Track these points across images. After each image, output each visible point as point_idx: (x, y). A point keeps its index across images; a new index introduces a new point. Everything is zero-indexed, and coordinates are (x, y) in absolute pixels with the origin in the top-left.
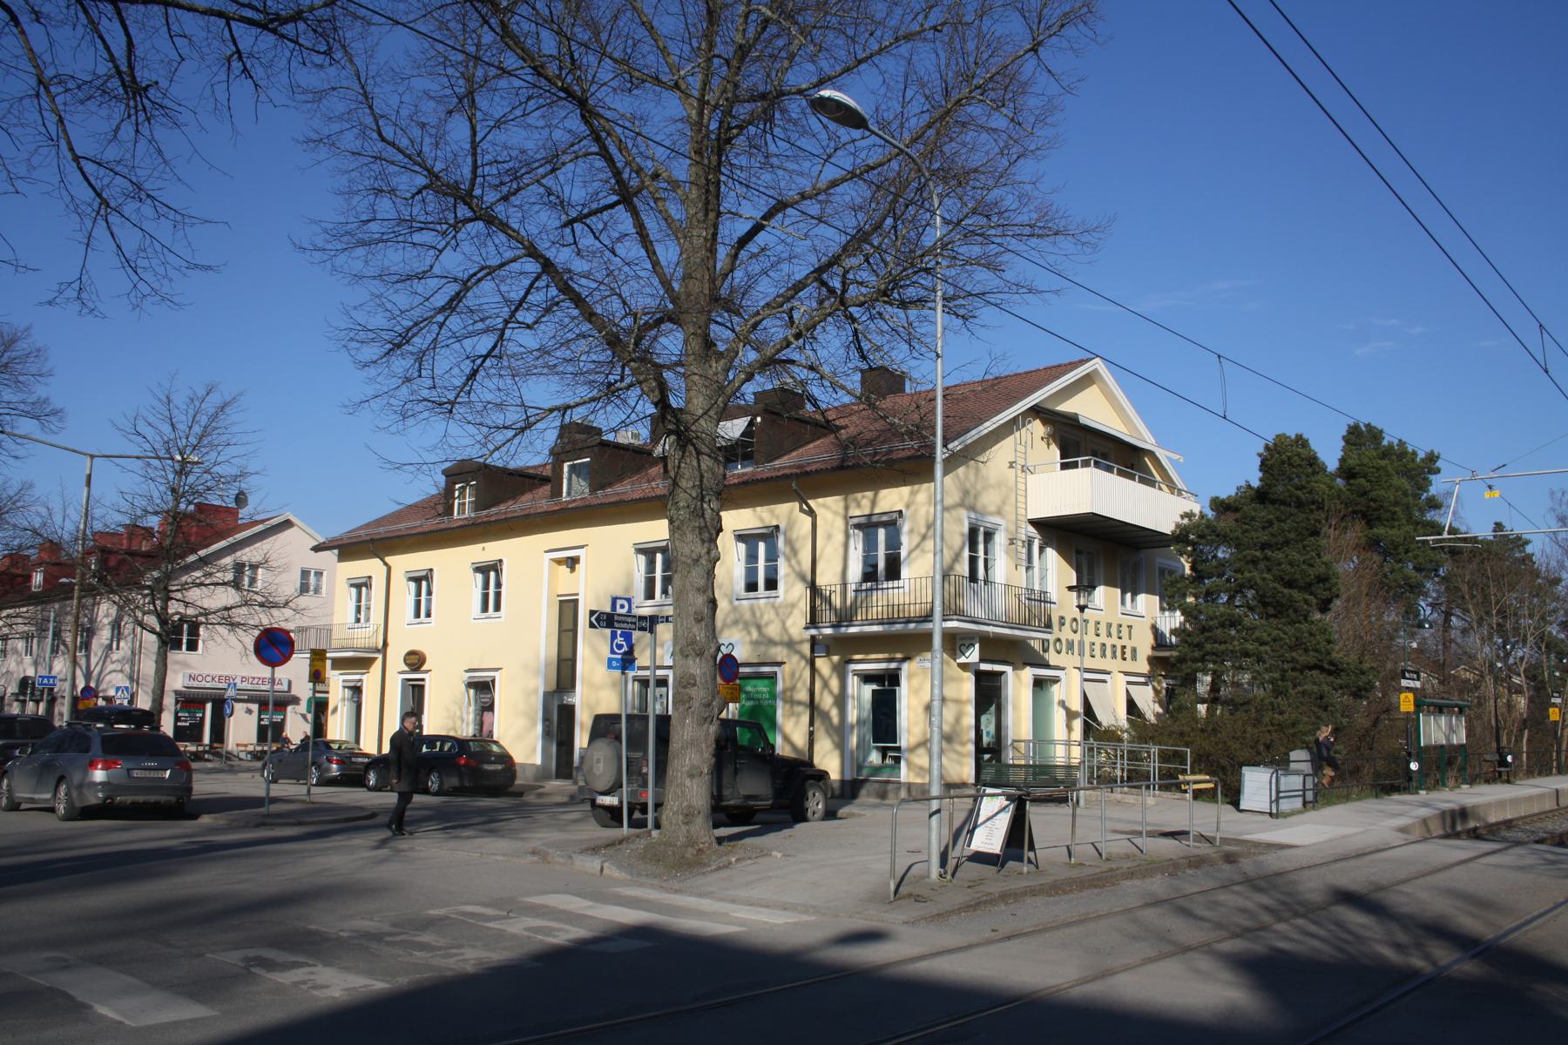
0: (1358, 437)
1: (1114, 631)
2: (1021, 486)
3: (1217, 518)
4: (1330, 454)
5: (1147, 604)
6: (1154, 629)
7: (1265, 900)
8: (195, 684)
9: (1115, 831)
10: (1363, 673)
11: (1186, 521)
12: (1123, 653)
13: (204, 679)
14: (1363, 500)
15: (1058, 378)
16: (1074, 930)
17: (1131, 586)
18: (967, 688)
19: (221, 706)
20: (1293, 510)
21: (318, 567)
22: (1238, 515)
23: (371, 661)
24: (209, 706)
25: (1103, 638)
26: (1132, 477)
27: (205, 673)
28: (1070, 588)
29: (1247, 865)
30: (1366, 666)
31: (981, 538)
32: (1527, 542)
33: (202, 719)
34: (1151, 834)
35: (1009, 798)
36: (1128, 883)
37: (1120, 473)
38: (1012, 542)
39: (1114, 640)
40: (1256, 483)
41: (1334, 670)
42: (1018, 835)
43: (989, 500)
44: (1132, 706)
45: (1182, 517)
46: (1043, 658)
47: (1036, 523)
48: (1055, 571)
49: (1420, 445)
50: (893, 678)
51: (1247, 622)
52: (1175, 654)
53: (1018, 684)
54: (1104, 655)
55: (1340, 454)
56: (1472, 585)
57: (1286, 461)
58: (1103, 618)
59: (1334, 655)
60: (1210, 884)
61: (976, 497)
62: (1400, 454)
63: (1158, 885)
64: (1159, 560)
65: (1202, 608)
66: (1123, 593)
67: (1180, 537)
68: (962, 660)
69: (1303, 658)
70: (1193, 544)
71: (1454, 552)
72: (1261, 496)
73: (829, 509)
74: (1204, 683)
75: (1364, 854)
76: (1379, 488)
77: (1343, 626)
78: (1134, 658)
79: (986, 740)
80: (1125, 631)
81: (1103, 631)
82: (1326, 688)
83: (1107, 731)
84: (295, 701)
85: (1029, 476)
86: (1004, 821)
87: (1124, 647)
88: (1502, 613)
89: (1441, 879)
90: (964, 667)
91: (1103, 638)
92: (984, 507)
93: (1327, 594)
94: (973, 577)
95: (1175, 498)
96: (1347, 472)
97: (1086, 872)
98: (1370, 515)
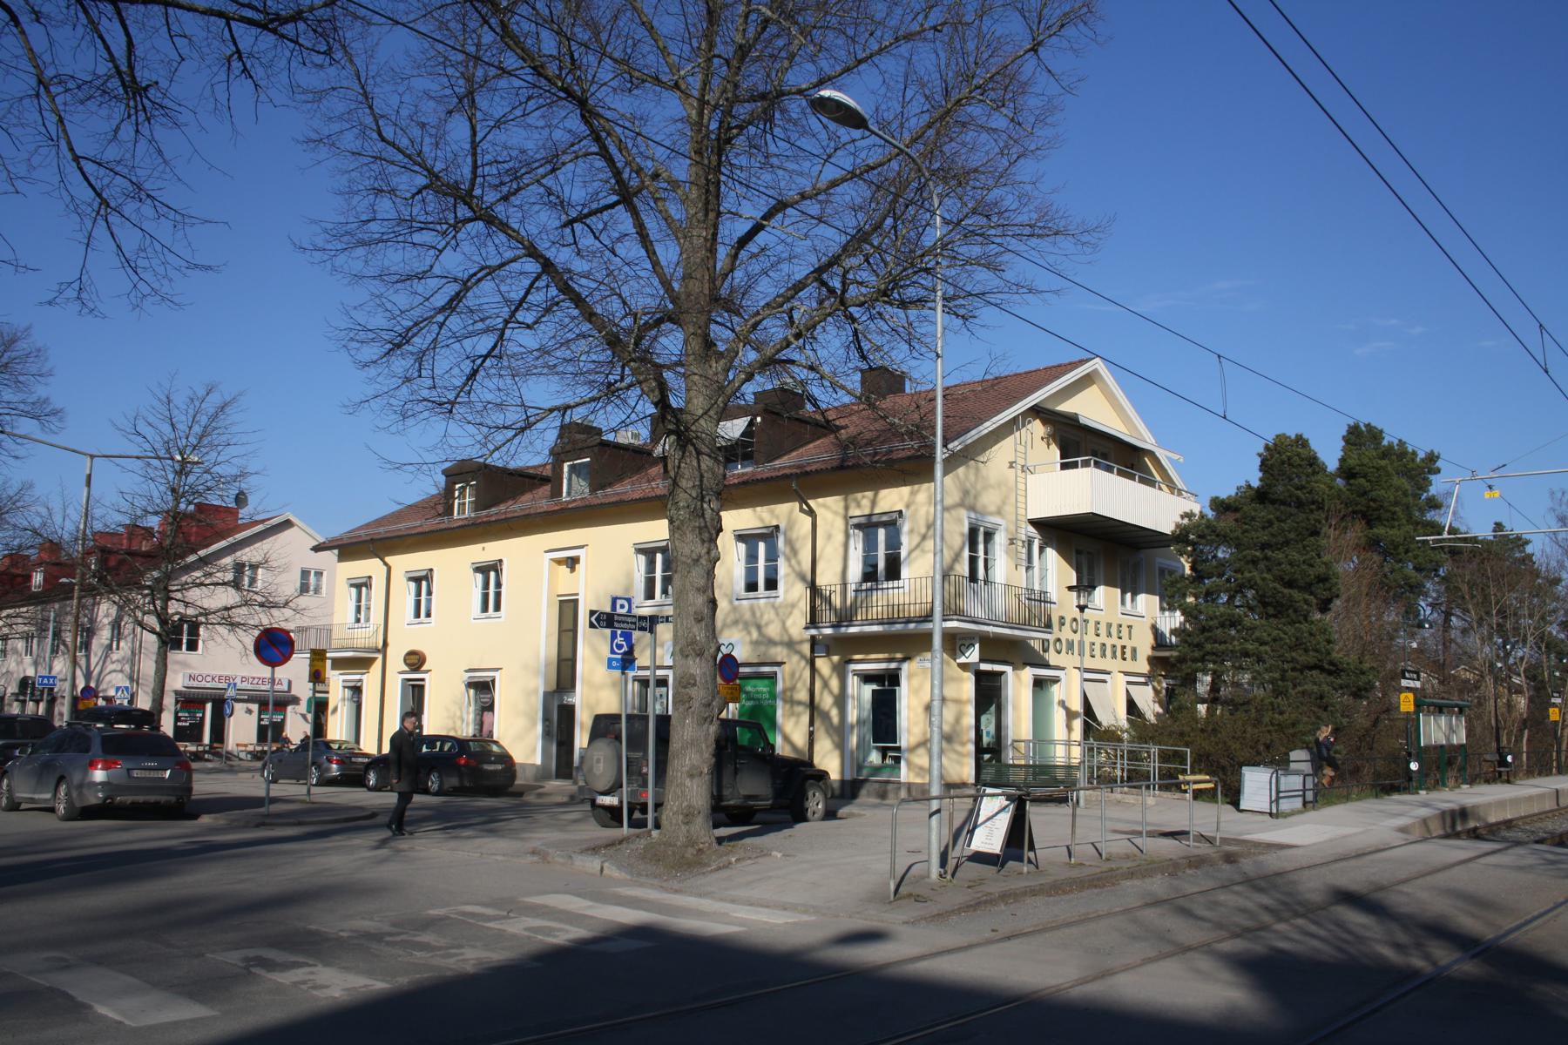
0: (1358, 437)
1: (1114, 631)
2: (1021, 486)
3: (1217, 518)
4: (1330, 454)
5: (1147, 604)
6: (1154, 629)
7: (1265, 900)
8: (195, 684)
9: (1115, 831)
10: (1363, 673)
11: (1186, 521)
12: (1123, 653)
13: (204, 679)
14: (1363, 500)
15: (1058, 378)
16: (1074, 930)
17: (1131, 586)
18: (967, 688)
19: (221, 706)
20: (1293, 510)
21: (318, 567)
22: (1238, 515)
23: (371, 661)
24: (209, 706)
25: (1103, 638)
26: (1132, 477)
27: (205, 673)
28: (1070, 588)
29: (1247, 865)
30: (1366, 666)
31: (981, 538)
32: (1527, 542)
33: (202, 719)
34: (1151, 834)
35: (1009, 798)
36: (1128, 883)
37: (1120, 473)
38: (1012, 542)
39: (1114, 640)
40: (1256, 483)
41: (1334, 670)
42: (1018, 835)
43: (989, 500)
44: (1132, 706)
45: (1182, 517)
46: (1043, 658)
47: (1036, 523)
48: (1055, 571)
49: (1420, 445)
50: (893, 678)
51: (1247, 622)
52: (1175, 654)
53: (1018, 684)
54: (1104, 655)
55: (1340, 454)
56: (1472, 585)
57: (1286, 461)
58: (1103, 618)
59: (1334, 655)
60: (1210, 884)
61: (976, 497)
62: (1400, 454)
63: (1158, 885)
64: (1159, 560)
65: (1202, 608)
66: (1123, 593)
67: (1180, 537)
68: (962, 660)
69: (1303, 658)
70: (1193, 544)
71: (1454, 552)
72: (1261, 496)
73: (829, 509)
74: (1204, 683)
75: (1364, 854)
76: (1379, 488)
77: (1343, 626)
78: (1134, 658)
79: (986, 740)
80: (1125, 631)
81: (1103, 631)
82: (1326, 688)
83: (1107, 731)
84: (295, 701)
85: (1029, 476)
86: (1004, 821)
87: (1124, 647)
88: (1502, 613)
89: (1441, 879)
90: (964, 667)
91: (1103, 638)
92: (984, 507)
93: (1327, 594)
94: (973, 577)
95: (1175, 498)
96: (1347, 472)
97: (1086, 872)
98: (1370, 515)
